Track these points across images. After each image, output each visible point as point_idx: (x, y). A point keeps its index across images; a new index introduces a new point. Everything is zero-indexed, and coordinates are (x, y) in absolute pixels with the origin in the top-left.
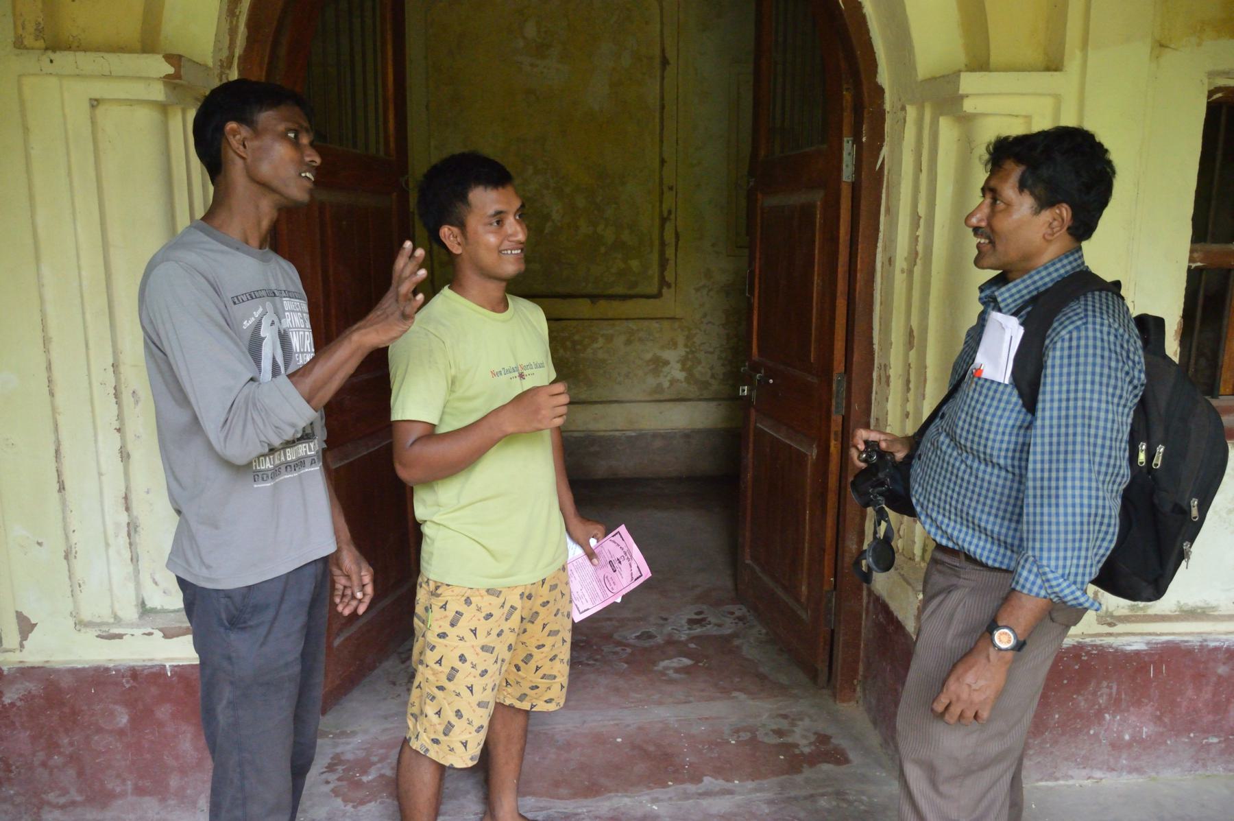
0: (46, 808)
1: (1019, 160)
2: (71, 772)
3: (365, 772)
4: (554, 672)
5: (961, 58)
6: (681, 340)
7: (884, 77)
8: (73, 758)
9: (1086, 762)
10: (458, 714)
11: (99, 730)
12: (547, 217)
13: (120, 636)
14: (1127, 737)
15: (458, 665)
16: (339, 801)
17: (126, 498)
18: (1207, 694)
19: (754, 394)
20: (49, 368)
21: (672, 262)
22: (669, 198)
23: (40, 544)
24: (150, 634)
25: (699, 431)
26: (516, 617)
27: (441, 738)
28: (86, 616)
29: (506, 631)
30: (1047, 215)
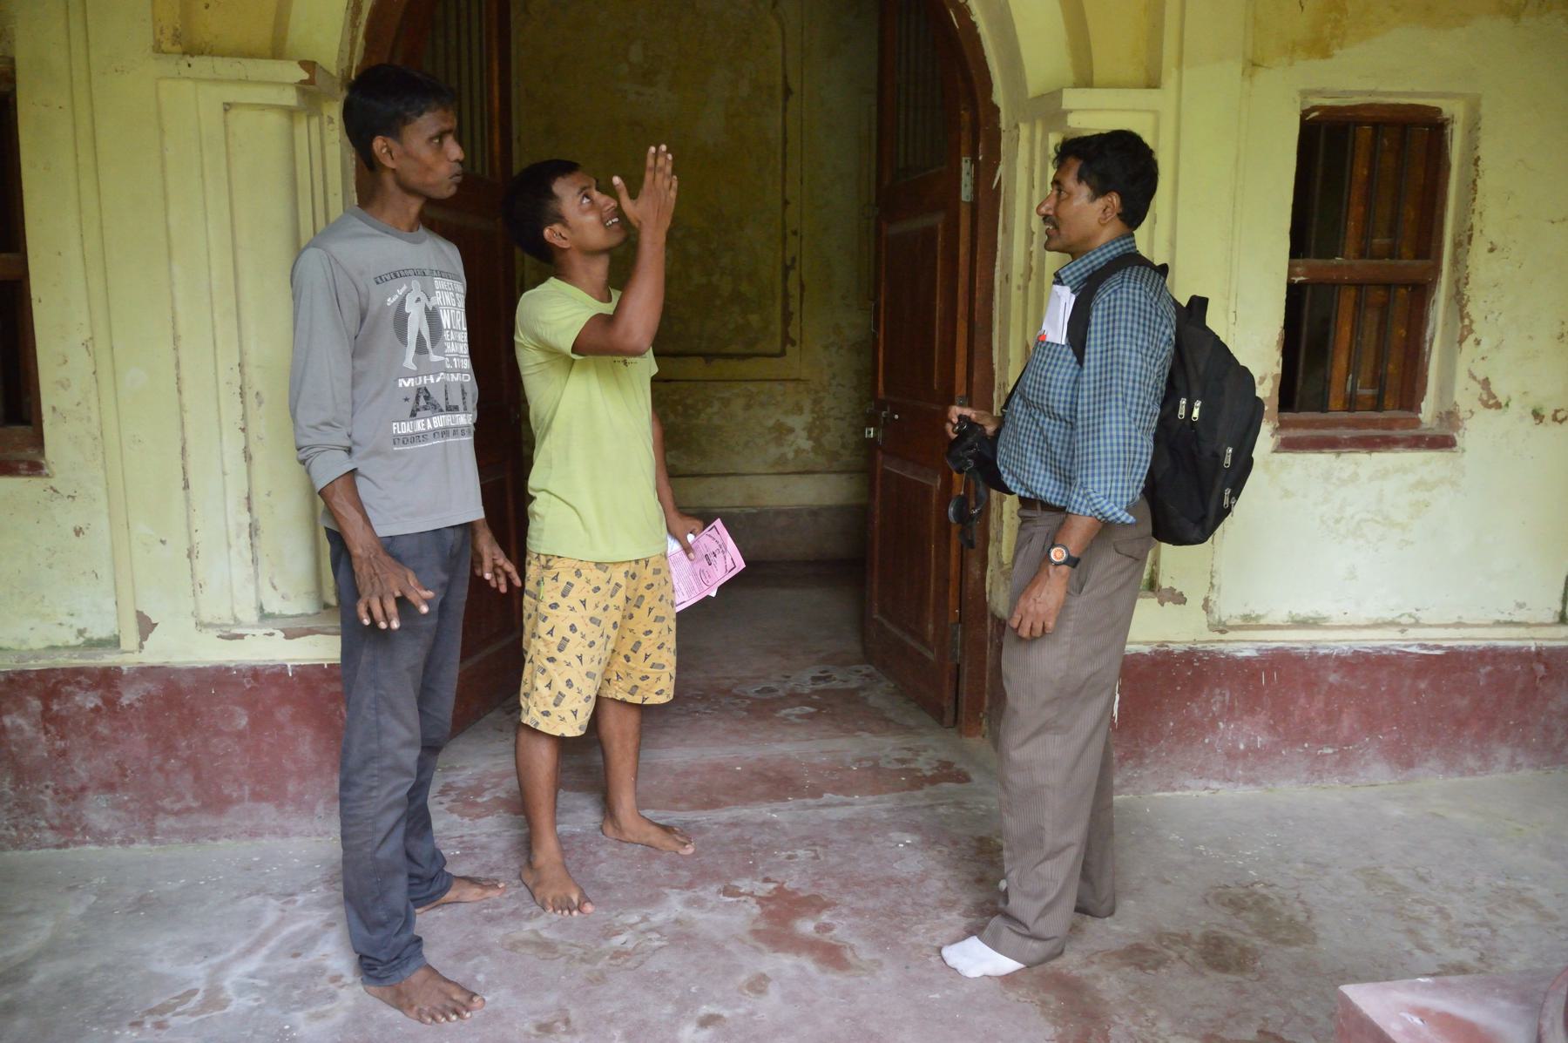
0: (161, 815)
1: (1078, 156)
2: (188, 777)
3: (479, 795)
4: (662, 661)
5: (1070, 76)
6: (807, 404)
7: (999, 96)
8: (192, 763)
9: (1202, 772)
10: (569, 683)
11: (219, 733)
13: (241, 637)
14: (1242, 747)
15: (569, 634)
16: (455, 817)
17: (248, 498)
18: (1319, 703)
19: (880, 435)
20: (178, 365)
21: (796, 317)
23: (163, 542)
24: (271, 634)
25: (829, 508)
26: (621, 594)
27: (552, 709)
28: (206, 617)
29: (612, 608)
30: (1100, 203)
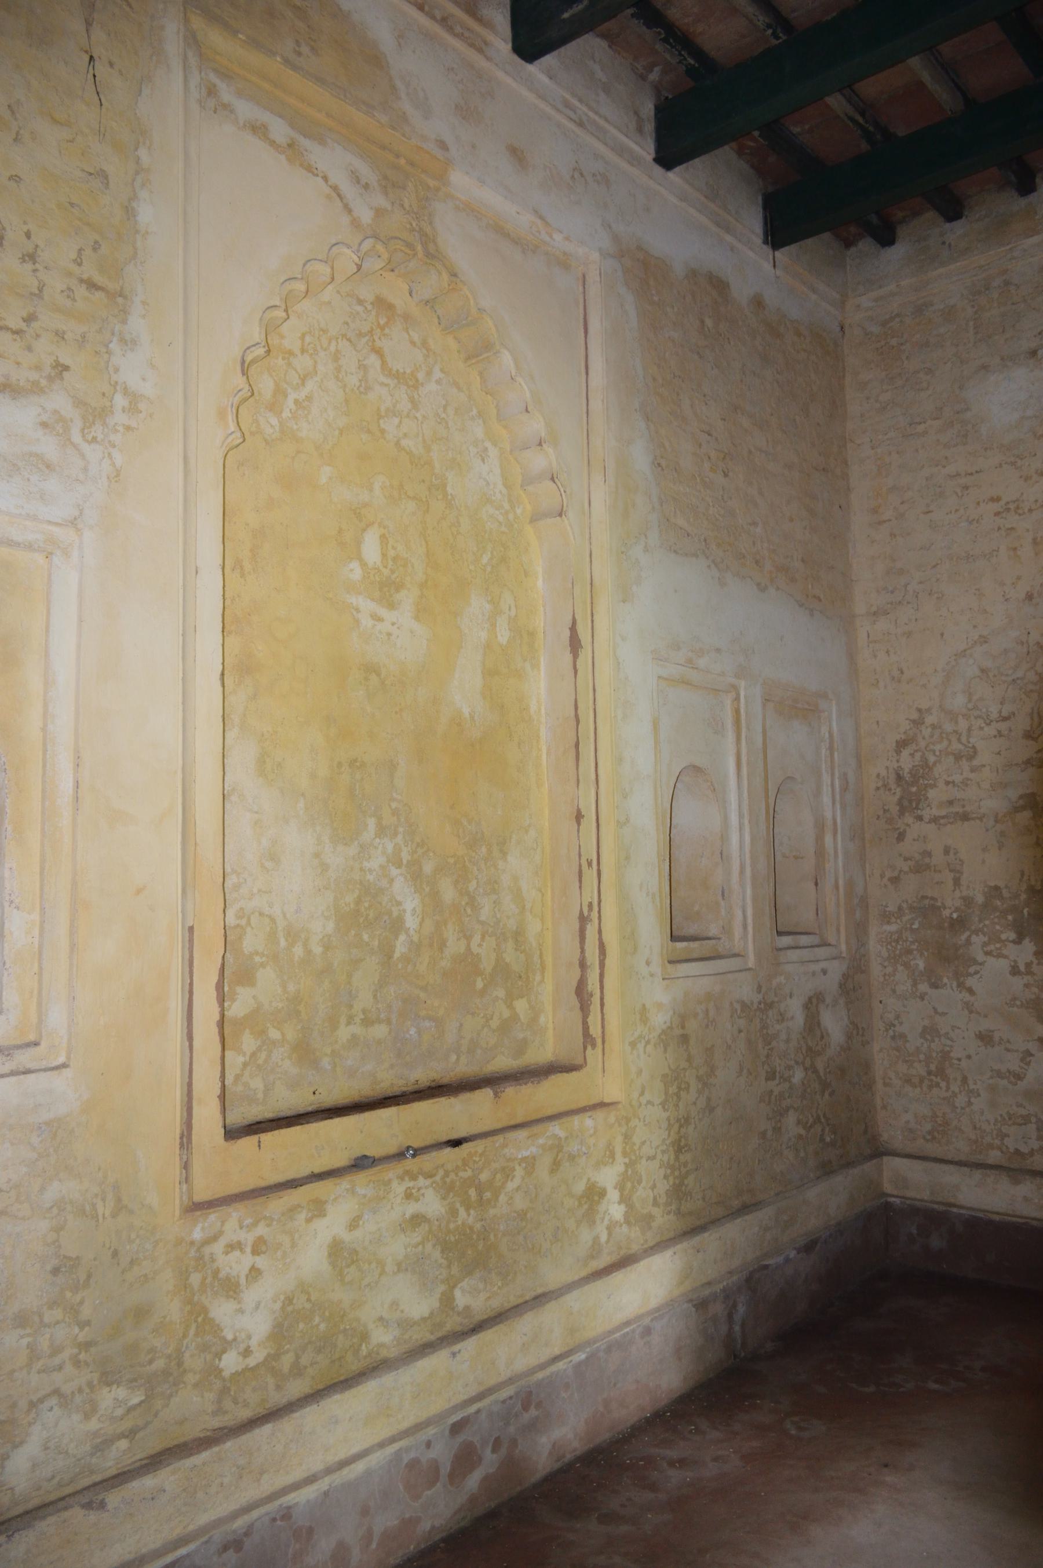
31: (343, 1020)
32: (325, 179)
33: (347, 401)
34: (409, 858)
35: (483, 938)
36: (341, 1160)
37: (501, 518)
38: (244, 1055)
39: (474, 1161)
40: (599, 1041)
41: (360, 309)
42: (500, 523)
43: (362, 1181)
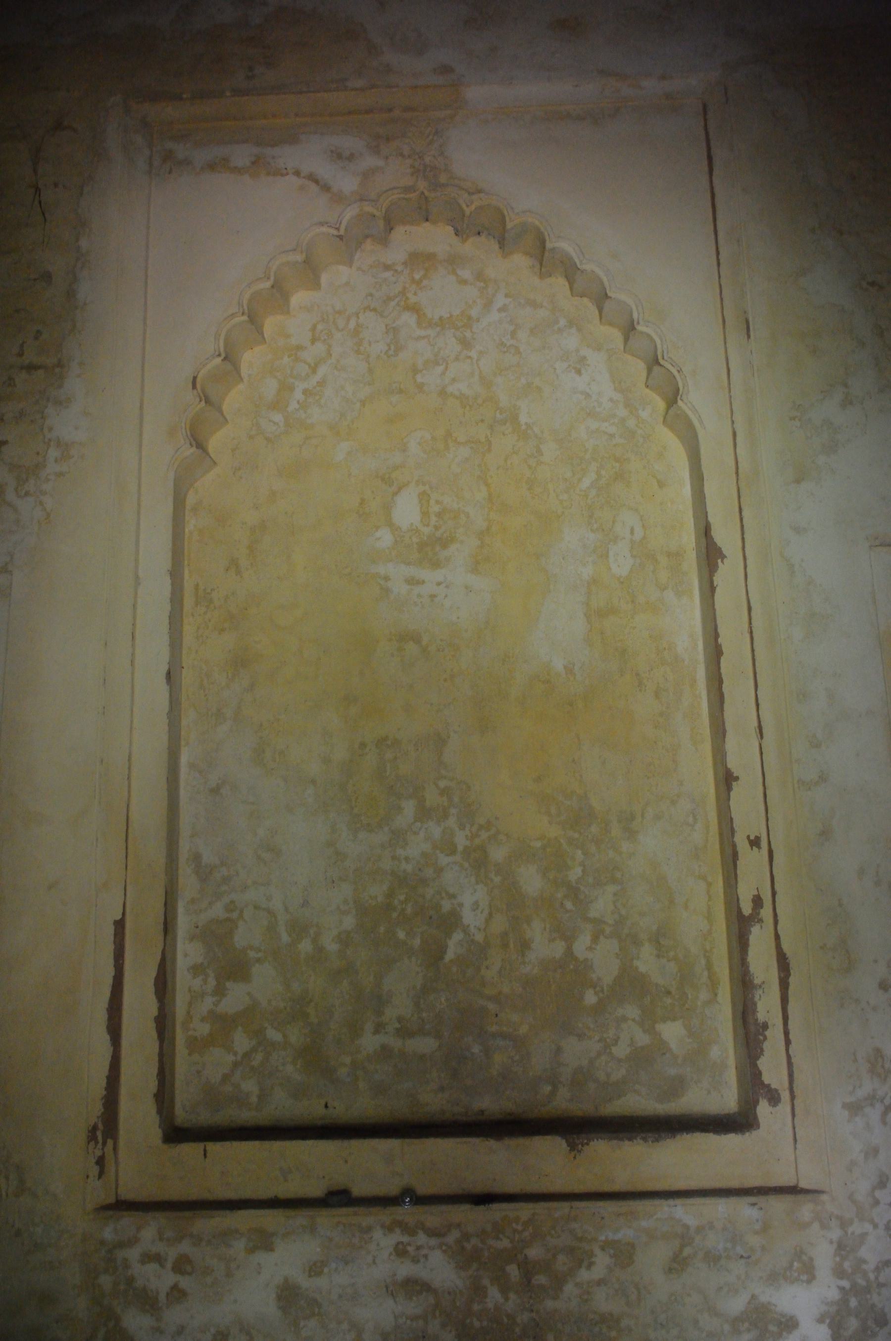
12: (450, 922)
21: (775, 1034)
22: (751, 862)
31: (369, 1027)
32: (297, 173)
33: (371, 371)
34: (468, 843)
35: (595, 939)
36: (316, 1190)
37: (612, 430)
38: (235, 1054)
39: (515, 1231)
40: (785, 1095)
41: (387, 274)
42: (612, 436)
43: (326, 1221)
